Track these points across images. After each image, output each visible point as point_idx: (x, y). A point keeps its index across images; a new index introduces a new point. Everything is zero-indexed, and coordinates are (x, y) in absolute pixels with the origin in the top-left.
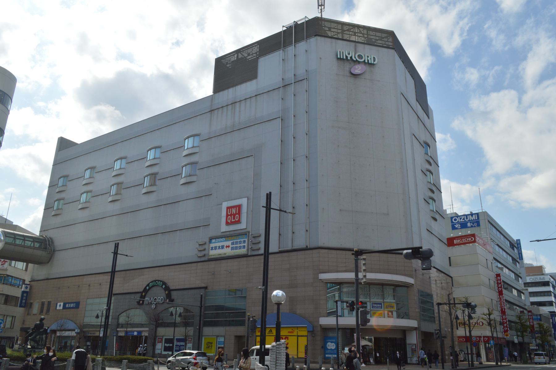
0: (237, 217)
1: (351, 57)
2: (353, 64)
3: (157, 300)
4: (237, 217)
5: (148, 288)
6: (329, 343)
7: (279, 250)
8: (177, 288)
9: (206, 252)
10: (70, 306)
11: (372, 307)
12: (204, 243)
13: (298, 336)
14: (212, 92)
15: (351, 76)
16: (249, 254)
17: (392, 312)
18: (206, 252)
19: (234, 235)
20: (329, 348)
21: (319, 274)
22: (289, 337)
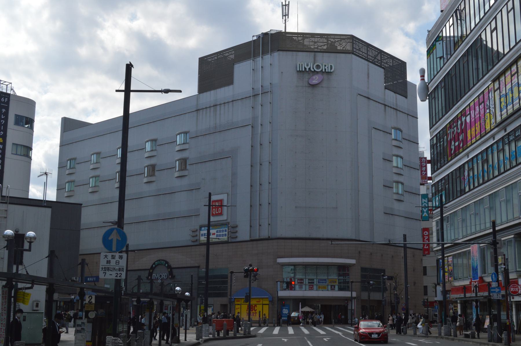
0: (220, 210)
1: (310, 69)
2: (311, 74)
3: (162, 276)
4: (220, 210)
5: (154, 266)
6: (284, 310)
7: (251, 239)
8: (177, 266)
9: (198, 238)
10: (91, 280)
11: (318, 282)
12: (196, 230)
13: (263, 304)
14: (197, 92)
15: (309, 87)
16: (230, 241)
17: (334, 286)
18: (198, 238)
19: (218, 225)
20: (284, 313)
21: (277, 259)
22: (257, 305)
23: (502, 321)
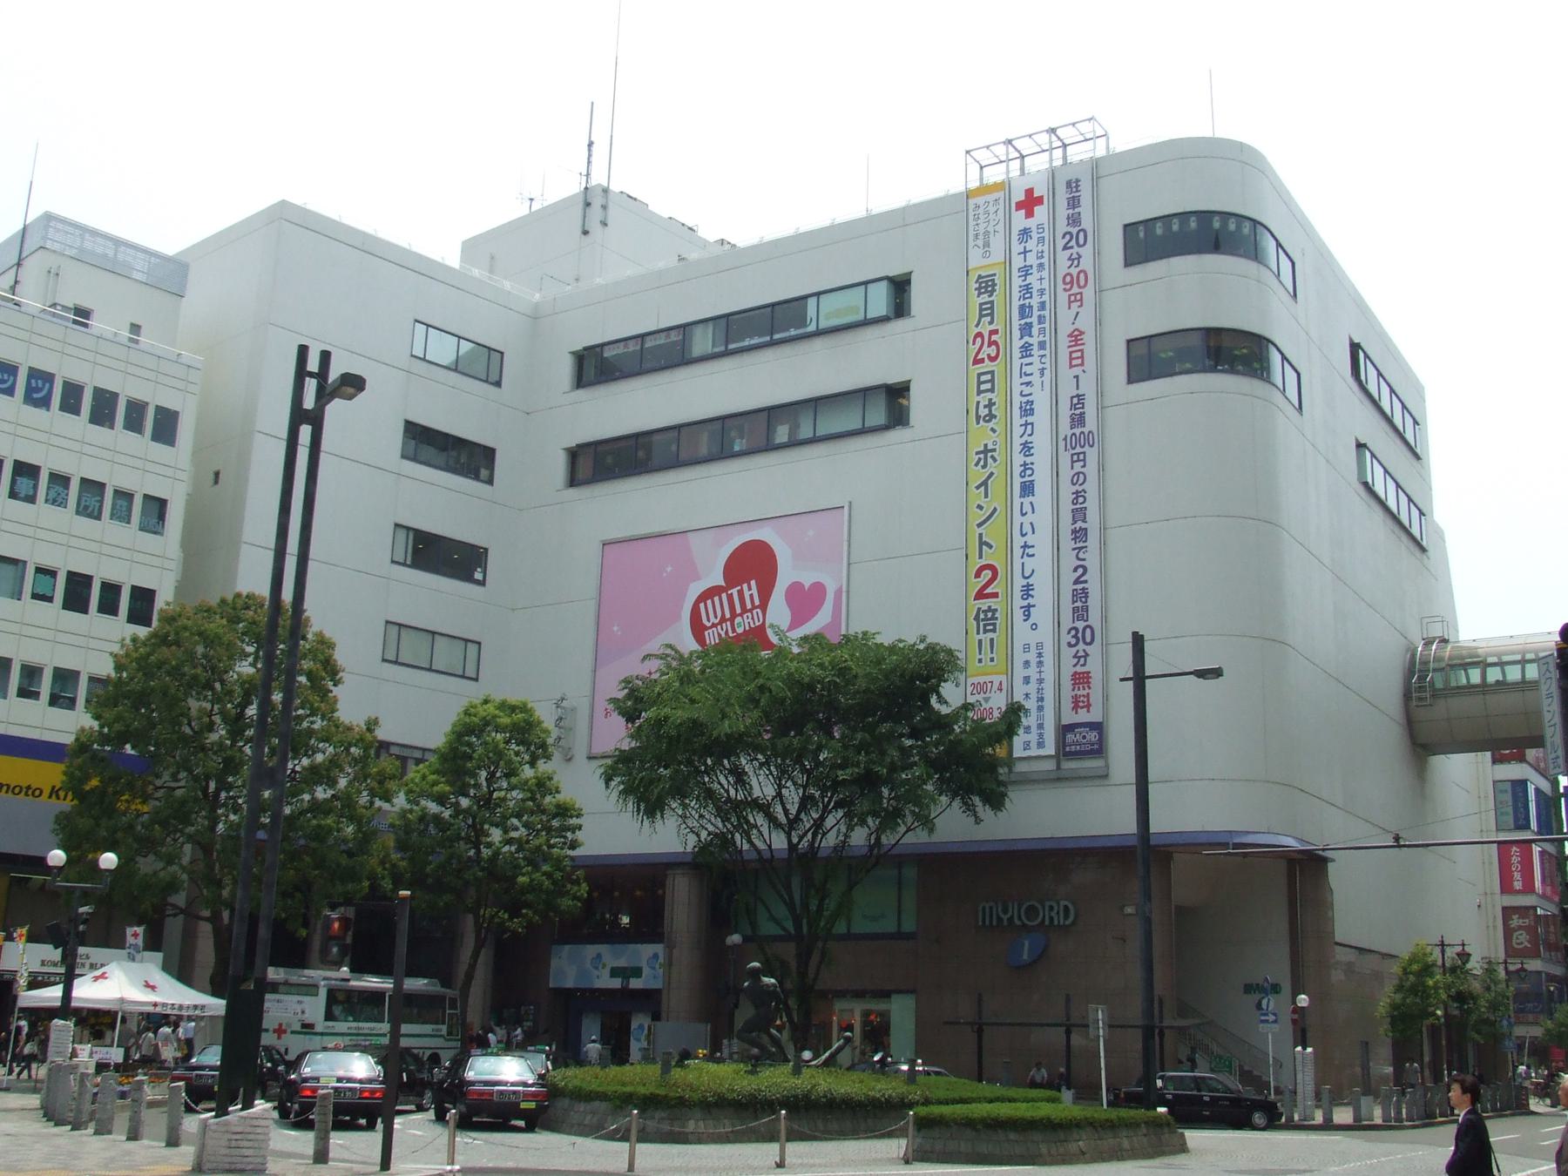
1: (1011, 919)
23: (73, 1004)
